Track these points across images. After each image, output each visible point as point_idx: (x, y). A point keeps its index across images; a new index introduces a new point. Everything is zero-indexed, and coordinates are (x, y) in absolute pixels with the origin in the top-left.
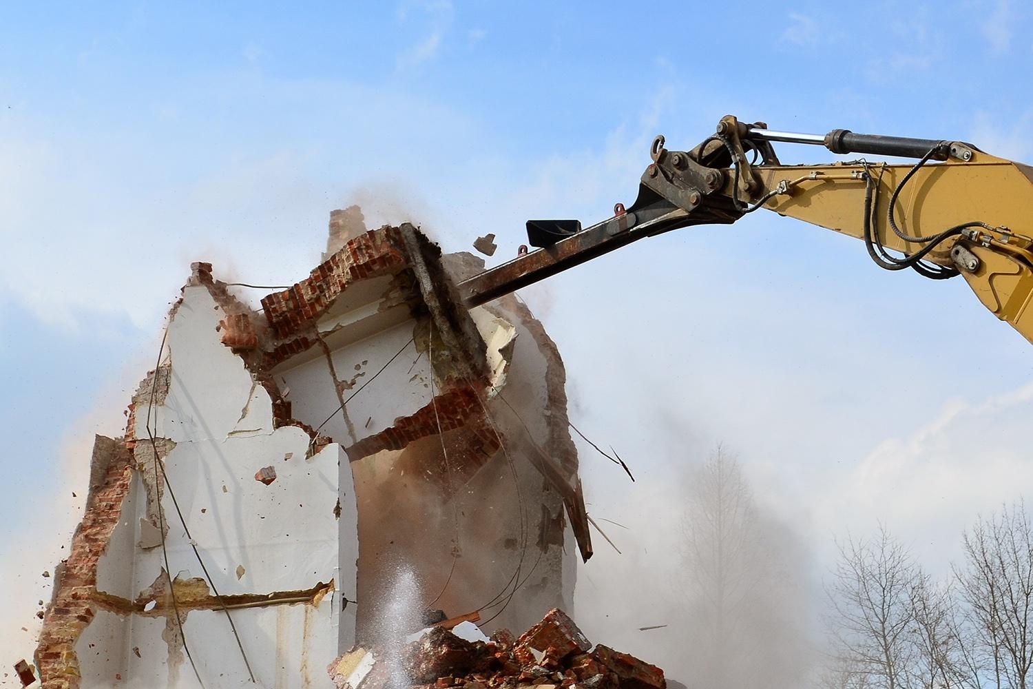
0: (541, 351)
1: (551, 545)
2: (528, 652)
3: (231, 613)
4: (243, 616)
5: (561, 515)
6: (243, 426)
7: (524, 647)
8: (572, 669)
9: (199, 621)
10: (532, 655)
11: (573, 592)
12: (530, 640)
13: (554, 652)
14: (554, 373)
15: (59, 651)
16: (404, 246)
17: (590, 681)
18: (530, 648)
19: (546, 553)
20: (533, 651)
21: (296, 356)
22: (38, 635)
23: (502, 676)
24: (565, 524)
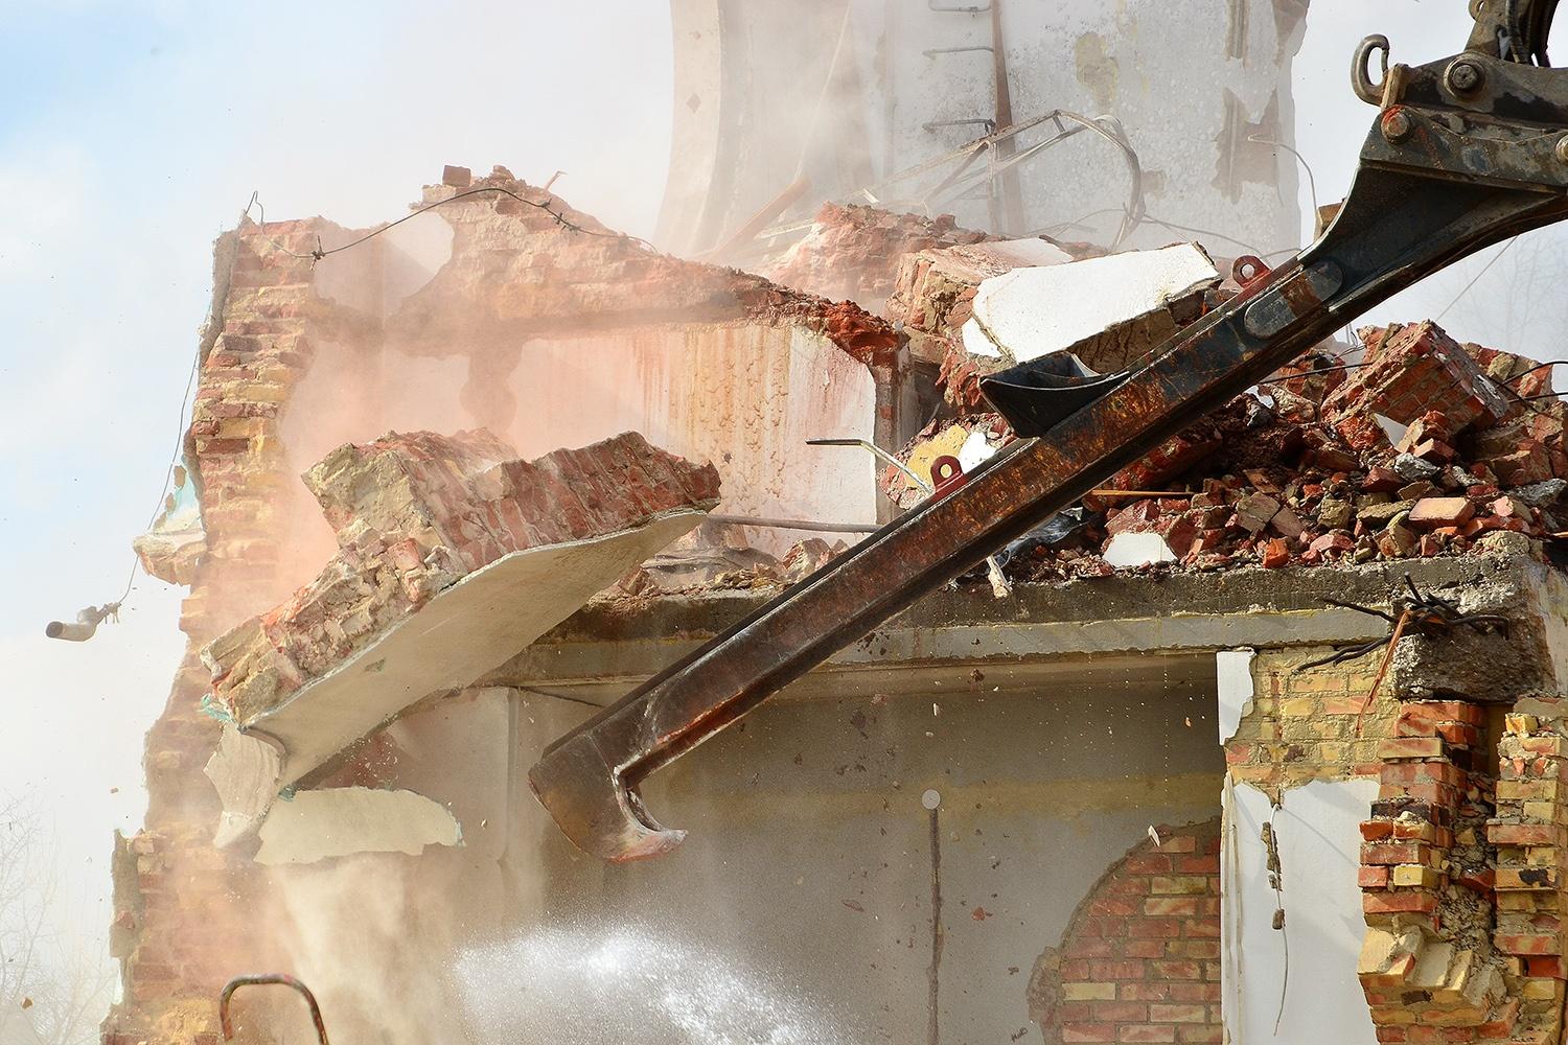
1: (1246, 185)
2: (1369, 424)
7: (1359, 413)
8: (1488, 463)
10: (1381, 430)
12: (1375, 398)
13: (1440, 420)
15: (246, 433)
16: (256, 323)
17: (1535, 490)
18: (1376, 415)
19: (1235, 202)
20: (1383, 422)
21: (195, 388)
23: (1316, 480)
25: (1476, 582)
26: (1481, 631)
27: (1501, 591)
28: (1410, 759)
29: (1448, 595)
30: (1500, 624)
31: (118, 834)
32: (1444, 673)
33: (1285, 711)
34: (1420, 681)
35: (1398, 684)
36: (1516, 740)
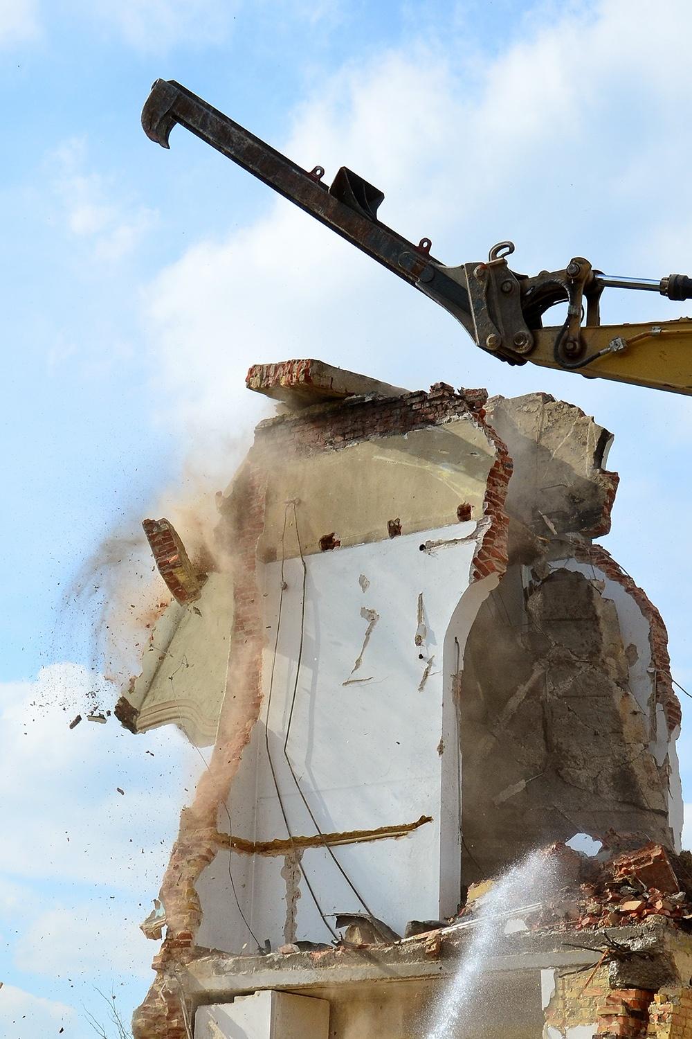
0: (644, 615)
3: (335, 849)
4: (341, 851)
5: (632, 664)
6: (355, 676)
9: (313, 857)
11: (680, 834)
14: (656, 634)
22: (528, 863)
24: (671, 770)
25: (641, 937)
26: (644, 958)
27: (651, 940)
28: (611, 1015)
29: (629, 942)
30: (648, 955)
31: (333, 534)
32: (629, 977)
33: (568, 996)
34: (619, 981)
35: (610, 982)
36: (656, 1008)
